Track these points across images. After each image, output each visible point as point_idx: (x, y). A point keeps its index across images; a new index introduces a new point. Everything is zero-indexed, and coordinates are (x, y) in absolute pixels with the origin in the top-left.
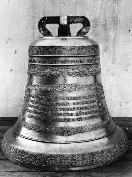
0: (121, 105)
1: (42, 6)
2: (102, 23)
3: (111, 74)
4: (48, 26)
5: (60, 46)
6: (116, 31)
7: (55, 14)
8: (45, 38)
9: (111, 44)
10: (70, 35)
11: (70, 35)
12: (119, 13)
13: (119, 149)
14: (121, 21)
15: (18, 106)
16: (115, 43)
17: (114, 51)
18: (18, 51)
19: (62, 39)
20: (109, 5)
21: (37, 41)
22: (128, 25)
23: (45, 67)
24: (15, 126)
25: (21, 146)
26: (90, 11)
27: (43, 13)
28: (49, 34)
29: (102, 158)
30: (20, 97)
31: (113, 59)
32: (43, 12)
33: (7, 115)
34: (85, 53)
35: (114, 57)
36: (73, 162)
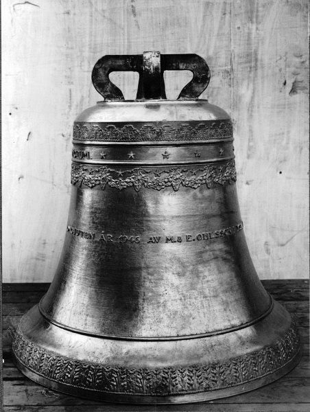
0: (268, 251)
1: (88, 32)
2: (224, 68)
3: (245, 181)
4: (116, 78)
5: (139, 122)
6: (254, 84)
7: (117, 49)
8: (109, 103)
9: (245, 114)
10: (164, 97)
11: (164, 97)
12: (260, 44)
13: (284, 349)
14: (266, 61)
15: (37, 259)
16: (252, 111)
17: (251, 131)
18: (34, 135)
19: (148, 107)
20: (239, 28)
21: (91, 111)
22: (280, 70)
23: (131, 169)
24: (45, 300)
25: (54, 346)
26: (196, 40)
27: (90, 48)
28: (116, 94)
29: (236, 376)
30: (40, 239)
31: (250, 148)
32: (90, 45)
33: (12, 280)
34: (212, 136)
35: (251, 144)
36: (195, 381)
